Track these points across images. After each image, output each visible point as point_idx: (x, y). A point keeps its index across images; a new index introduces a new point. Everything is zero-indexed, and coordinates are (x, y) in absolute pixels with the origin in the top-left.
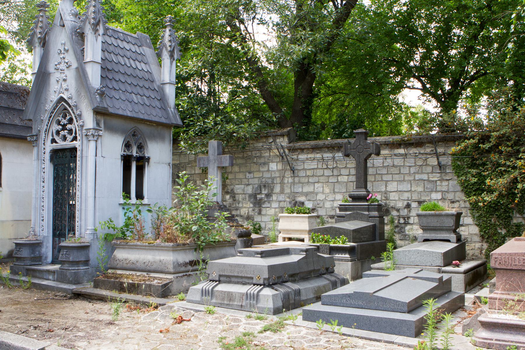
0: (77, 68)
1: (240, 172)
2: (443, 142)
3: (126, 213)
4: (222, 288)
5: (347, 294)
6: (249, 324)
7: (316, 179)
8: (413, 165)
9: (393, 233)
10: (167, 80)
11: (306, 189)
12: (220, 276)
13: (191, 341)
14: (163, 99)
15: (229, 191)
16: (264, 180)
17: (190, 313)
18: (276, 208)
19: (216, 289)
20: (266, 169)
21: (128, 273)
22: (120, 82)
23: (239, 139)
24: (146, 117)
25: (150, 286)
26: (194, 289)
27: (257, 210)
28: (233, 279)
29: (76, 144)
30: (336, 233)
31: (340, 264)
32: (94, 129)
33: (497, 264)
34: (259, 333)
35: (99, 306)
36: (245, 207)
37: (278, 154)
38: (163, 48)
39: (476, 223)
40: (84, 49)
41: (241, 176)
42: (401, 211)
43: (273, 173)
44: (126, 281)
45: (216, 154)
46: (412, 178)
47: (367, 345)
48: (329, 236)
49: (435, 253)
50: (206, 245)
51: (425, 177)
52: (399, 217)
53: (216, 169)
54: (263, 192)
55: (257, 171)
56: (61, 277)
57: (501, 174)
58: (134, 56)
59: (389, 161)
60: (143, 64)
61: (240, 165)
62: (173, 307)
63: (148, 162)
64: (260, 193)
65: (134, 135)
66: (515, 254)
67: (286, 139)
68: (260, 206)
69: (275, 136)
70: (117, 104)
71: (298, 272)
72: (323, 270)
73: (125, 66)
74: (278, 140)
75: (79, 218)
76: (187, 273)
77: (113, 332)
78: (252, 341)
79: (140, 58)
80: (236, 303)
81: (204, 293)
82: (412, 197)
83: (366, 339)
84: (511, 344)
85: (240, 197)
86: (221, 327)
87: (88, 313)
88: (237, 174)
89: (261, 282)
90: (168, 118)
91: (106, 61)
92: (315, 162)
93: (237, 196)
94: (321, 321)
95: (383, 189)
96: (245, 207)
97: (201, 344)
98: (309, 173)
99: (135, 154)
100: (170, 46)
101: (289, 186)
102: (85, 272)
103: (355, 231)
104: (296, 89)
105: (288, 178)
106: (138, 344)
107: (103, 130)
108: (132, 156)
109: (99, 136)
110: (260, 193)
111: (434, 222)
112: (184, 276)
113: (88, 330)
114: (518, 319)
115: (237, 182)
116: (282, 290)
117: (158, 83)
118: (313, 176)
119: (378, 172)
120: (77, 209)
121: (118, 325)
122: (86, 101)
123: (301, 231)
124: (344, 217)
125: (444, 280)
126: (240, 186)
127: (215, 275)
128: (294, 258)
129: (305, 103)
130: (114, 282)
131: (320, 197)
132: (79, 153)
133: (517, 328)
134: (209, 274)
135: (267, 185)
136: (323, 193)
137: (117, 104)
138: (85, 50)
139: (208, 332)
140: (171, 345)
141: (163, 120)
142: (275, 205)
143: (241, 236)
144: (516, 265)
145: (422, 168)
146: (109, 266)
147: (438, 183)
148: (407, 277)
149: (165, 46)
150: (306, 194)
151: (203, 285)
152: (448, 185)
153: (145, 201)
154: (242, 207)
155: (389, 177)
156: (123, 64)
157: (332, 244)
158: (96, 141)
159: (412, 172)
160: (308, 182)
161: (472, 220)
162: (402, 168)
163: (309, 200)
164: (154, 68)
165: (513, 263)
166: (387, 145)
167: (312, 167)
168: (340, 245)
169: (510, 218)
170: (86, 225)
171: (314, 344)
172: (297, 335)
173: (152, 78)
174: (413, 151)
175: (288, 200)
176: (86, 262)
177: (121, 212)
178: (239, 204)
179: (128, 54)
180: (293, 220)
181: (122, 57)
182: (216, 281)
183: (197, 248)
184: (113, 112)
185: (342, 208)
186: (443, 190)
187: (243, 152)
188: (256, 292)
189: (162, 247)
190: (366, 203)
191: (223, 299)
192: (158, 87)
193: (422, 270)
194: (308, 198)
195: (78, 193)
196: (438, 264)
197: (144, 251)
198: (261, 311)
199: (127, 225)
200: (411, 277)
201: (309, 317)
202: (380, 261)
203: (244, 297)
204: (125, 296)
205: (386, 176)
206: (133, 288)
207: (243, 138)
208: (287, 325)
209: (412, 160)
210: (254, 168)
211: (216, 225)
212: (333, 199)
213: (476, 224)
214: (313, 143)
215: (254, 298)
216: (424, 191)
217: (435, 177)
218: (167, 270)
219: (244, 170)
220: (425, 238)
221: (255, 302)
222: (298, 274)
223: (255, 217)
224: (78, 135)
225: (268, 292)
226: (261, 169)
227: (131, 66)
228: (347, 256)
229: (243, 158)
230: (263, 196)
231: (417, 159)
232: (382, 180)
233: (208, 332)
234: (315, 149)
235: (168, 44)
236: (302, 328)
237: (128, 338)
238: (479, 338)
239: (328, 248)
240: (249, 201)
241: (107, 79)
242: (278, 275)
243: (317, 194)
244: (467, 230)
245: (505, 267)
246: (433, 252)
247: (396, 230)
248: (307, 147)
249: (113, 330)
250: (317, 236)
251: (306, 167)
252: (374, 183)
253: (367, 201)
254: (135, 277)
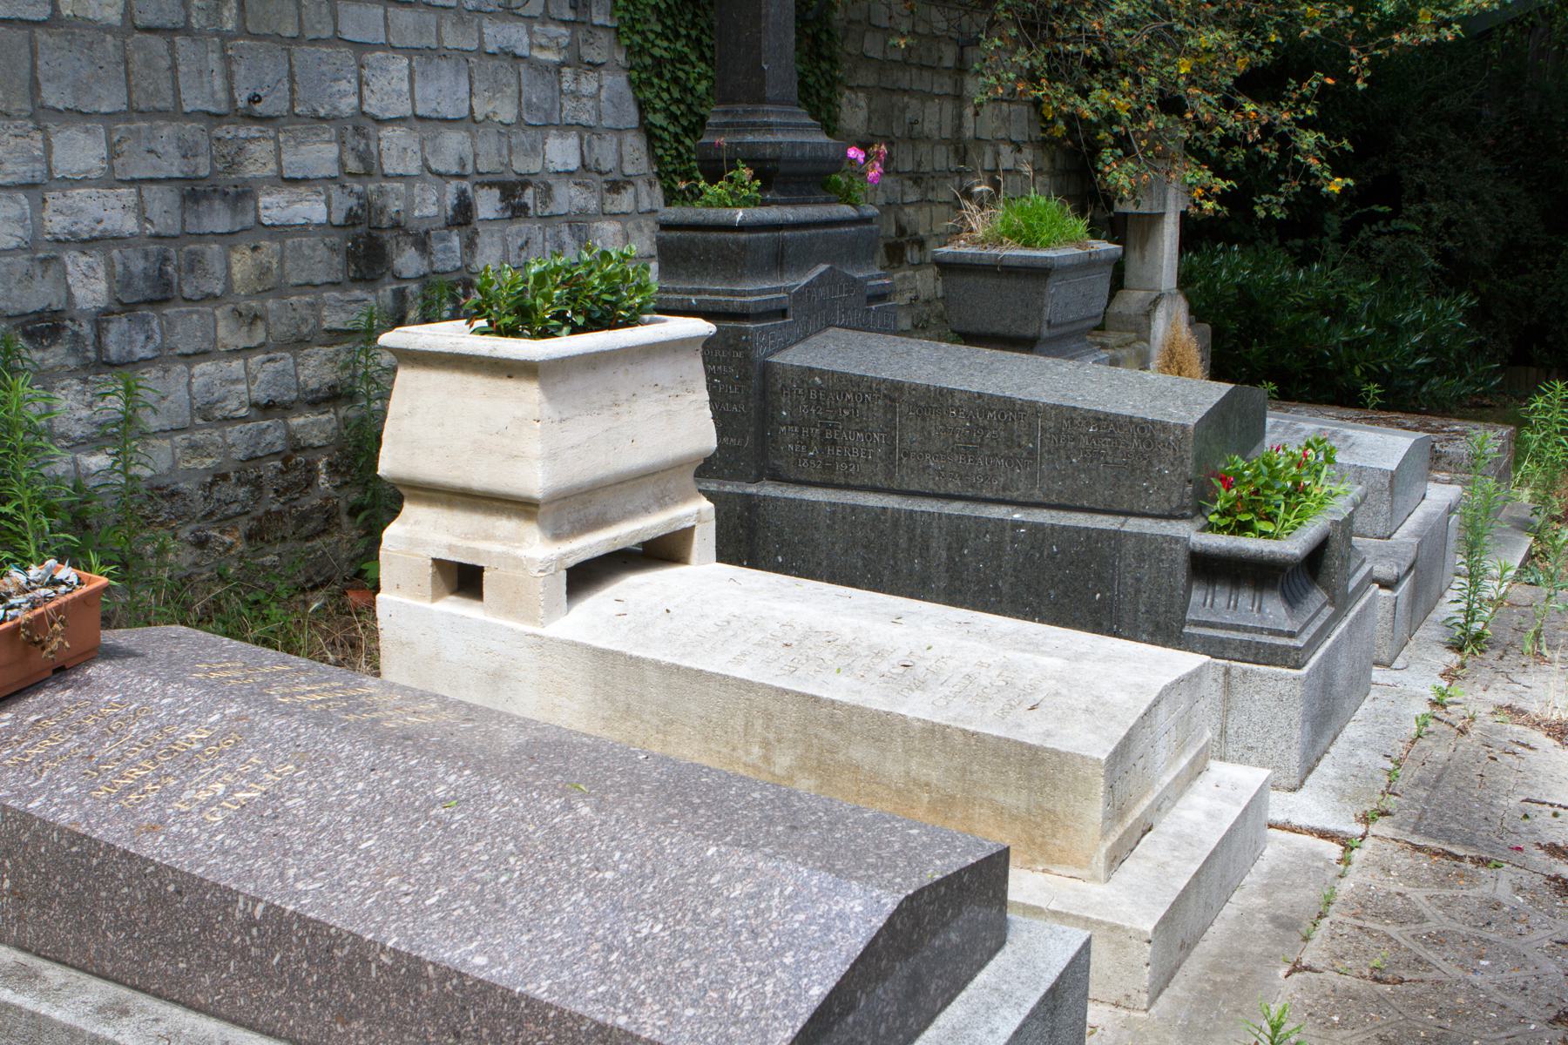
56: (1416, 1028)
95: (347, 105)
124: (783, 313)
232: (337, 40)
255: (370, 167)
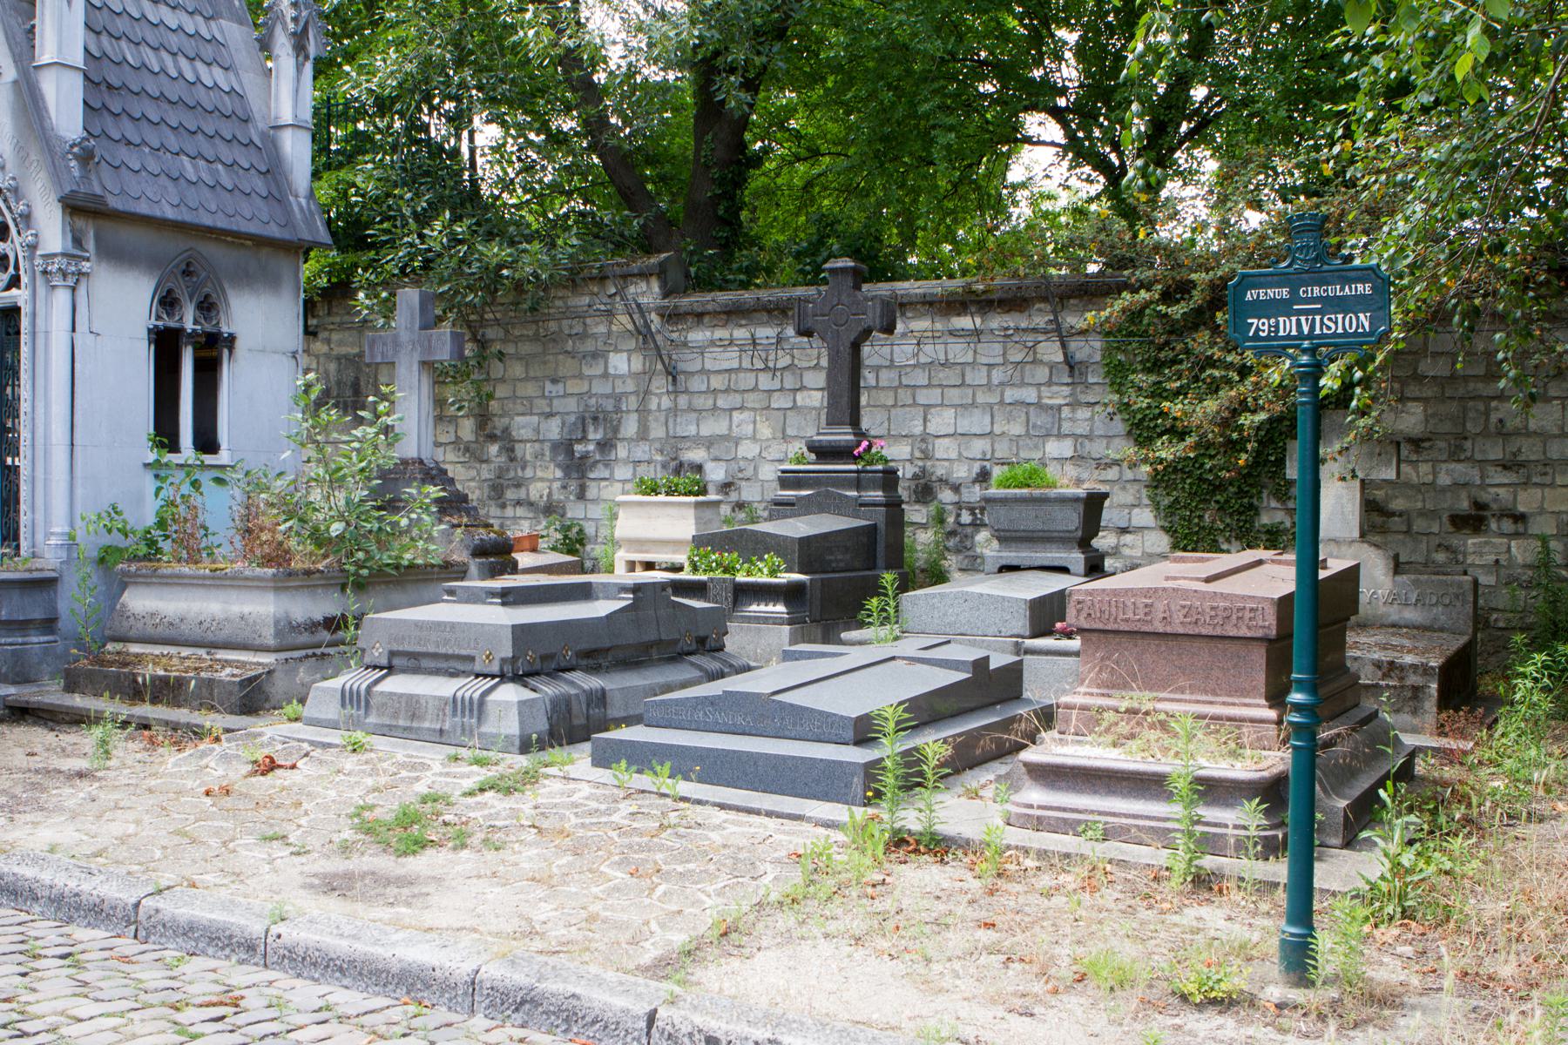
0: (15, 82)
1: (527, 379)
2: (1080, 297)
3: (159, 489)
4: (397, 684)
5: (706, 698)
6: (447, 774)
7: (736, 400)
8: (1000, 360)
9: (943, 551)
10: (287, 117)
11: (713, 427)
12: (392, 654)
13: (280, 814)
14: (274, 170)
15: (498, 432)
16: (593, 401)
17: (300, 748)
18: (624, 481)
19: (379, 688)
20: (599, 370)
21: (157, 652)
22: (144, 123)
23: (518, 286)
24: (222, 223)
25: (211, 682)
26: (324, 690)
27: (573, 486)
28: (425, 663)
29: (20, 296)
30: (753, 546)
31: (759, 630)
32: (64, 255)
33: (1082, 618)
34: (465, 794)
35: (69, 738)
36: (542, 480)
37: (630, 327)
38: (274, 26)
39: (1162, 523)
40: (33, 26)
41: (530, 389)
42: (963, 490)
43: (618, 382)
44: (149, 671)
45: (417, 326)
46: (994, 399)
47: (733, 823)
48: (735, 555)
49: (1009, 600)
50: (371, 575)
51: (1030, 395)
52: (959, 506)
53: (415, 367)
54: (591, 436)
55: (574, 377)
57: (1214, 388)
58: (190, 46)
59: (930, 351)
60: (217, 71)
61: (526, 359)
62: (260, 735)
63: (231, 349)
64: (584, 439)
65: (187, 273)
66: (1127, 591)
67: (655, 286)
68: (583, 476)
69: (626, 277)
70: (134, 186)
71: (608, 645)
72: (688, 643)
73: (162, 76)
74: (632, 289)
75: (29, 502)
76: (318, 651)
77: (82, 795)
78: (438, 814)
79: (208, 52)
80: (427, 725)
81: (349, 698)
82: (993, 451)
83: (738, 809)
84: (1090, 817)
85: (528, 451)
86: (370, 782)
87: (33, 755)
88: (519, 384)
89: (495, 668)
90: (288, 223)
91: (106, 61)
92: (733, 353)
93: (517, 446)
94: (623, 764)
95: (918, 430)
96: (542, 480)
97: (303, 821)
98: (717, 382)
99: (189, 325)
100: (295, 20)
101: (662, 419)
102: (46, 652)
103: (805, 542)
104: (699, 139)
105: (659, 396)
106: (138, 822)
107: (93, 258)
108: (182, 330)
109: (80, 273)
110: (584, 439)
111: (1027, 519)
112: (307, 657)
113: (18, 790)
114: (1123, 757)
115: (520, 409)
116: (549, 689)
117: (261, 125)
118: (727, 391)
119: (905, 382)
120: (22, 478)
121: (100, 779)
122: (43, 175)
123: (675, 544)
125: (992, 667)
126: (528, 418)
127: (378, 654)
128: (600, 608)
129: (721, 182)
130: (119, 674)
131: (747, 450)
132: (25, 323)
133: (1110, 777)
134: (363, 650)
135: (601, 416)
136: (754, 438)
137: (134, 186)
138: (37, 30)
139: (332, 794)
140: (225, 824)
141: (274, 231)
142: (622, 472)
143: (480, 551)
144: (1127, 620)
145: (1022, 371)
146: (107, 633)
147: (1066, 412)
148: (893, 658)
149: (280, 17)
150: (709, 442)
151: (353, 678)
152: (1092, 419)
153: (223, 457)
154: (533, 479)
155: (933, 396)
156: (157, 69)
157: (741, 578)
158: (74, 289)
159: (995, 381)
160: (715, 408)
161: (1151, 515)
162: (968, 369)
163: (716, 459)
164: (249, 82)
165: (1121, 616)
166: (931, 304)
167: (726, 365)
168: (763, 578)
169: (1254, 510)
170: (47, 522)
171: (595, 820)
172: (565, 799)
173: (245, 110)
174: (997, 321)
175: (659, 458)
176: (49, 624)
177: (150, 484)
178: (523, 469)
179: (174, 41)
180: (655, 511)
181: (155, 49)
182: (382, 668)
183: (343, 582)
184: (120, 207)
185: (788, 480)
186: (1079, 431)
187: (536, 322)
188: (476, 695)
189: (247, 579)
190: (853, 467)
191: (396, 715)
192: (264, 135)
193: (948, 642)
194: (715, 452)
195: (25, 434)
196: (1015, 631)
197: (201, 592)
198: (487, 743)
199: (161, 524)
200: (904, 658)
201: (602, 759)
202: (861, 625)
203: (449, 710)
204: (145, 710)
205: (925, 391)
206: (167, 690)
207: (529, 282)
208: (547, 776)
209: (997, 348)
210: (567, 366)
211: (404, 522)
212: (782, 456)
213: (1163, 528)
214: (724, 297)
215: (471, 710)
216: (1027, 434)
217: (1058, 396)
218: (257, 642)
219: (539, 374)
220: (1004, 562)
221: (474, 721)
222: (609, 649)
223: (569, 506)
224: (22, 272)
225: (510, 694)
226: (587, 371)
227: (181, 74)
228: (780, 608)
229: (536, 338)
230: (591, 447)
231: (1009, 345)
232: (915, 404)
233: (332, 794)
234: (733, 314)
235: (290, 13)
236: (584, 785)
237: (117, 807)
238: (1018, 805)
239: (730, 588)
240: (552, 460)
241: (105, 113)
242: (543, 652)
243: (737, 442)
244: (1139, 543)
245: (1101, 626)
246: (1004, 598)
247: (951, 543)
248: (710, 307)
249: (86, 788)
250: (706, 556)
251: (708, 366)
252: (893, 411)
253: (856, 459)
254: (175, 661)
255: (927, 456)
